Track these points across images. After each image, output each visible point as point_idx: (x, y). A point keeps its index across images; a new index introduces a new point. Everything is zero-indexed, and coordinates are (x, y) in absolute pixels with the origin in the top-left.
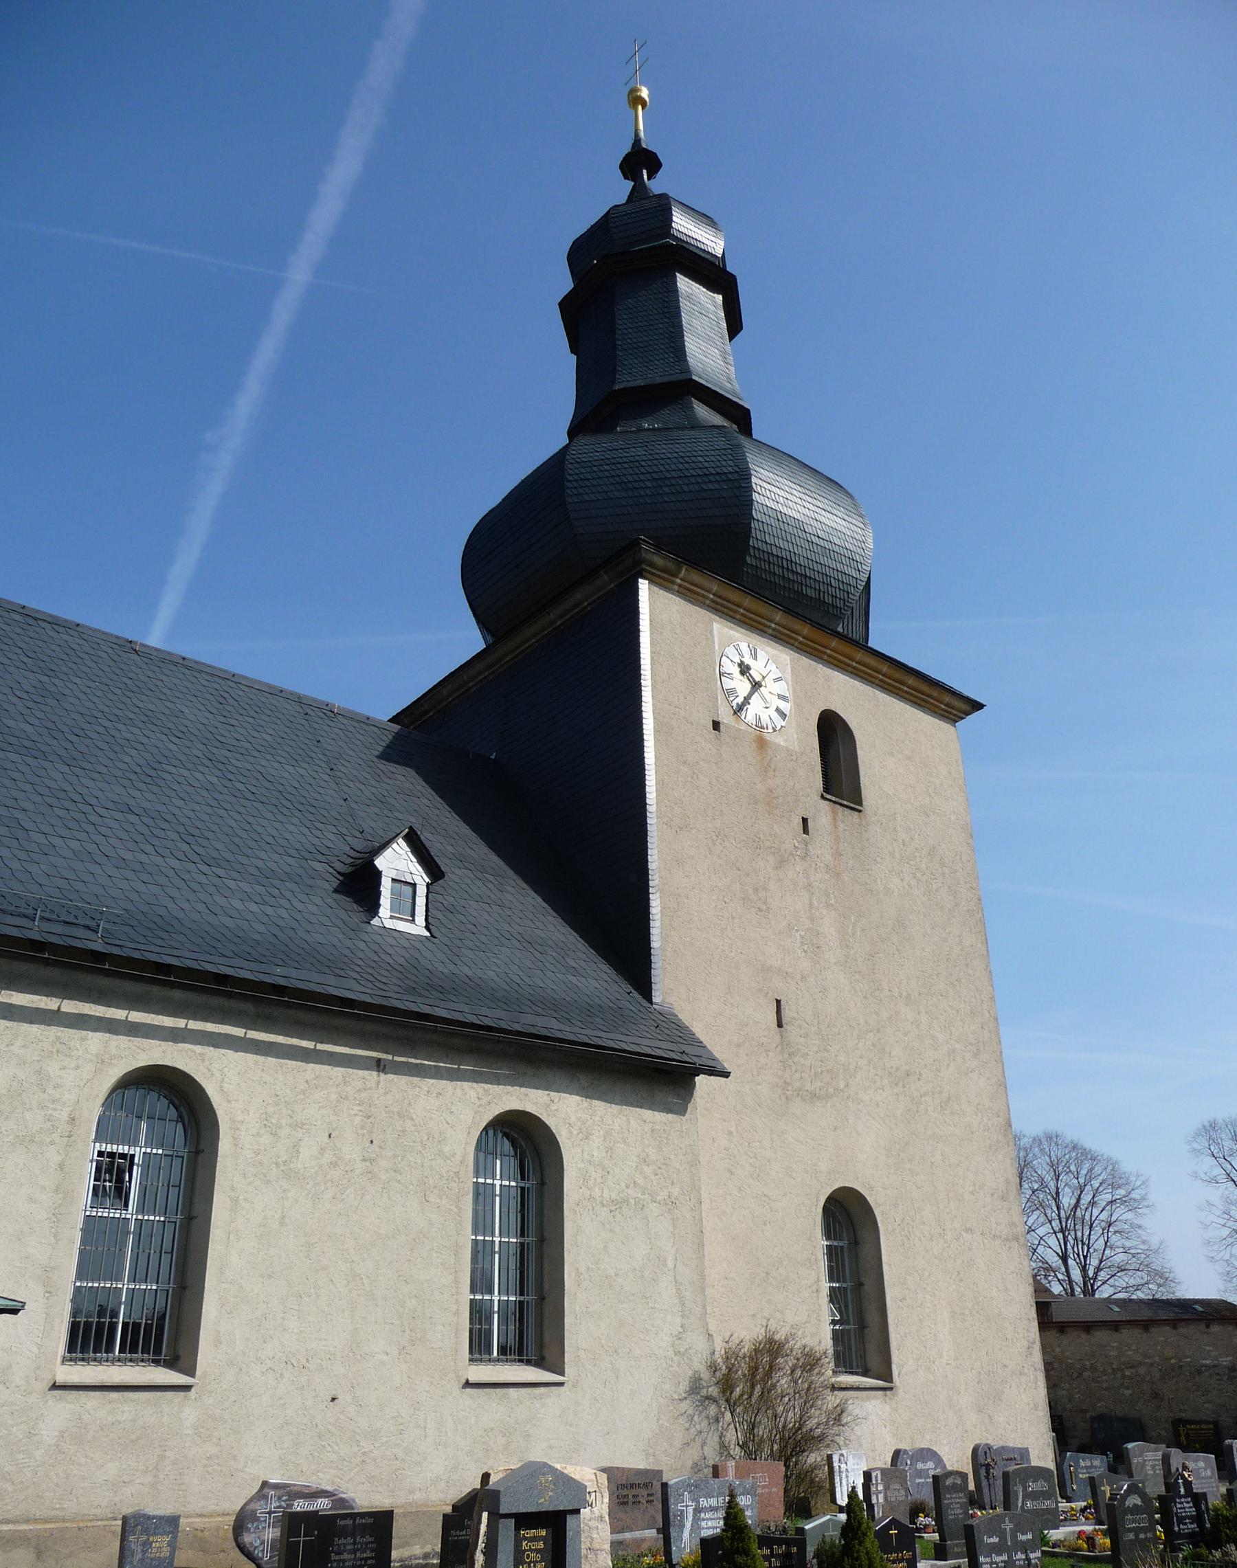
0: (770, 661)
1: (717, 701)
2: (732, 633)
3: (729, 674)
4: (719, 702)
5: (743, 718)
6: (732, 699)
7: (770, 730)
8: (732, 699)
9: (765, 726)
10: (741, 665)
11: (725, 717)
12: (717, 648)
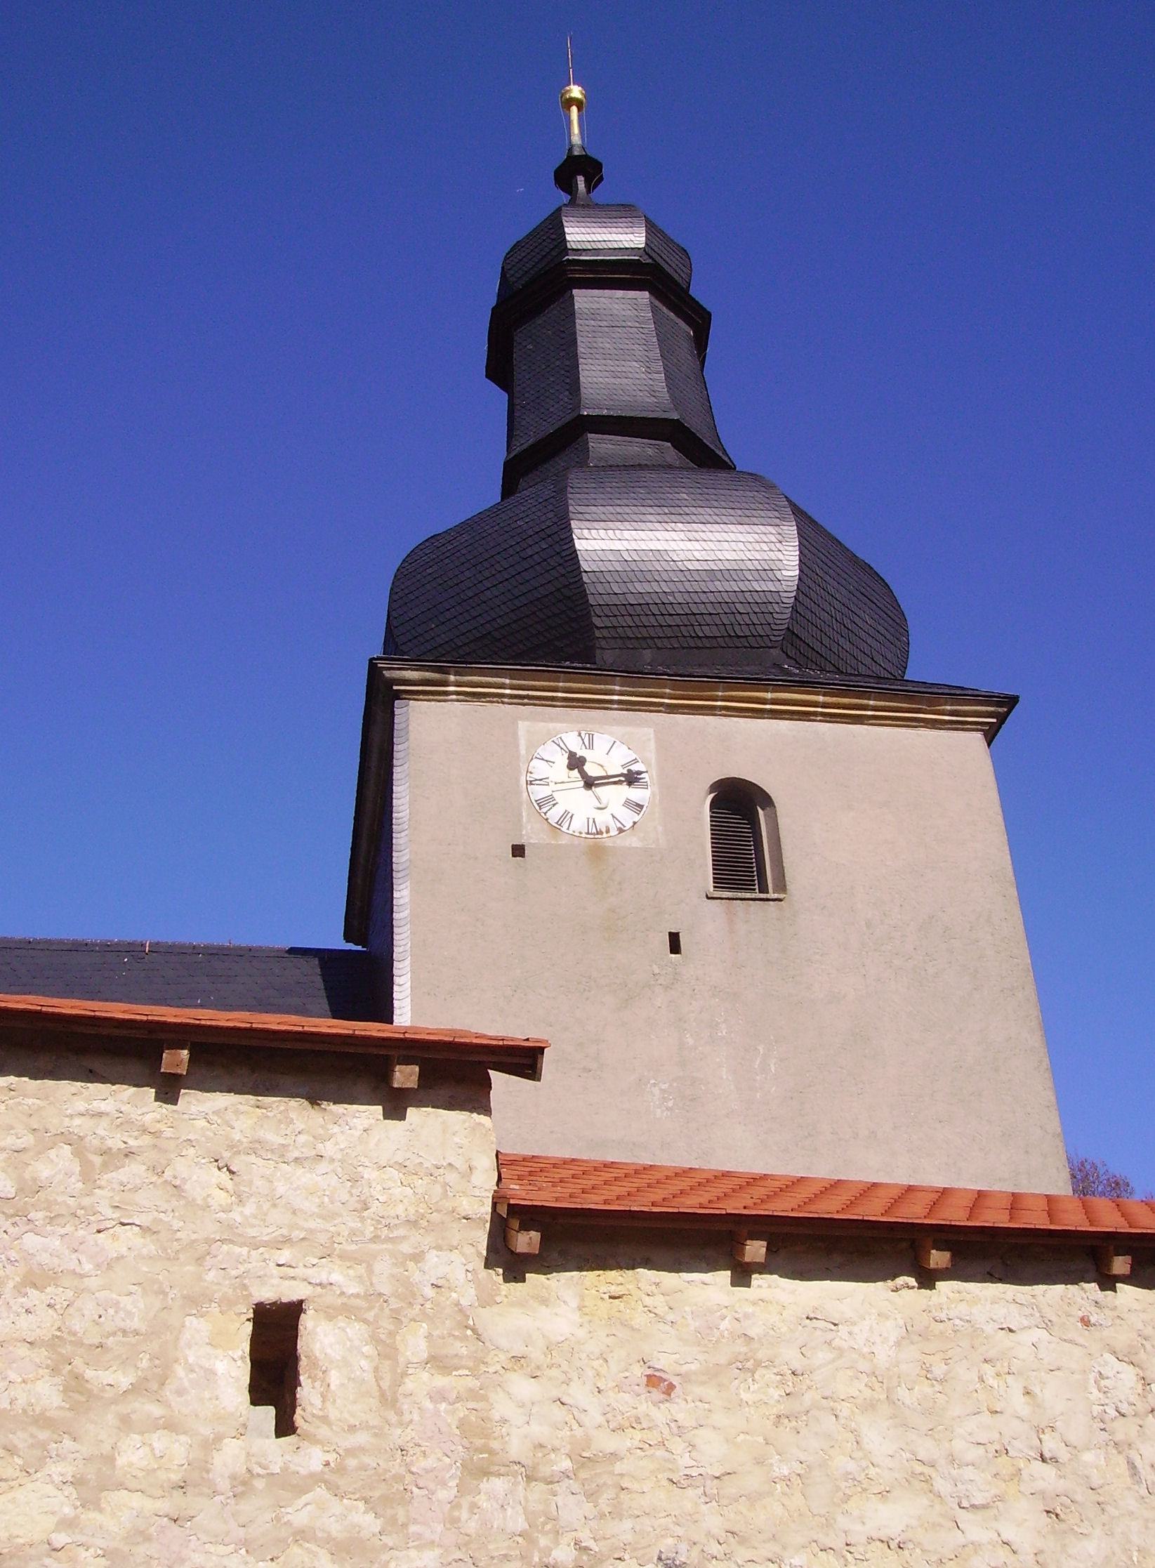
0: (618, 742)
1: (520, 820)
2: (551, 725)
3: (541, 780)
4: (524, 820)
5: (564, 829)
6: (544, 810)
7: (613, 832)
8: (544, 810)
9: (604, 830)
10: (572, 755)
11: (531, 835)
12: (523, 752)
